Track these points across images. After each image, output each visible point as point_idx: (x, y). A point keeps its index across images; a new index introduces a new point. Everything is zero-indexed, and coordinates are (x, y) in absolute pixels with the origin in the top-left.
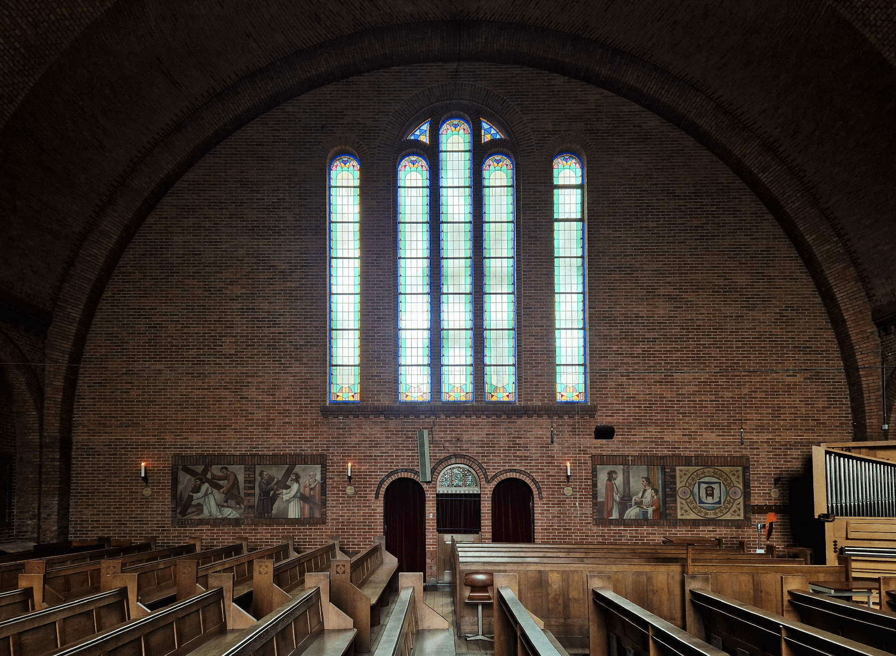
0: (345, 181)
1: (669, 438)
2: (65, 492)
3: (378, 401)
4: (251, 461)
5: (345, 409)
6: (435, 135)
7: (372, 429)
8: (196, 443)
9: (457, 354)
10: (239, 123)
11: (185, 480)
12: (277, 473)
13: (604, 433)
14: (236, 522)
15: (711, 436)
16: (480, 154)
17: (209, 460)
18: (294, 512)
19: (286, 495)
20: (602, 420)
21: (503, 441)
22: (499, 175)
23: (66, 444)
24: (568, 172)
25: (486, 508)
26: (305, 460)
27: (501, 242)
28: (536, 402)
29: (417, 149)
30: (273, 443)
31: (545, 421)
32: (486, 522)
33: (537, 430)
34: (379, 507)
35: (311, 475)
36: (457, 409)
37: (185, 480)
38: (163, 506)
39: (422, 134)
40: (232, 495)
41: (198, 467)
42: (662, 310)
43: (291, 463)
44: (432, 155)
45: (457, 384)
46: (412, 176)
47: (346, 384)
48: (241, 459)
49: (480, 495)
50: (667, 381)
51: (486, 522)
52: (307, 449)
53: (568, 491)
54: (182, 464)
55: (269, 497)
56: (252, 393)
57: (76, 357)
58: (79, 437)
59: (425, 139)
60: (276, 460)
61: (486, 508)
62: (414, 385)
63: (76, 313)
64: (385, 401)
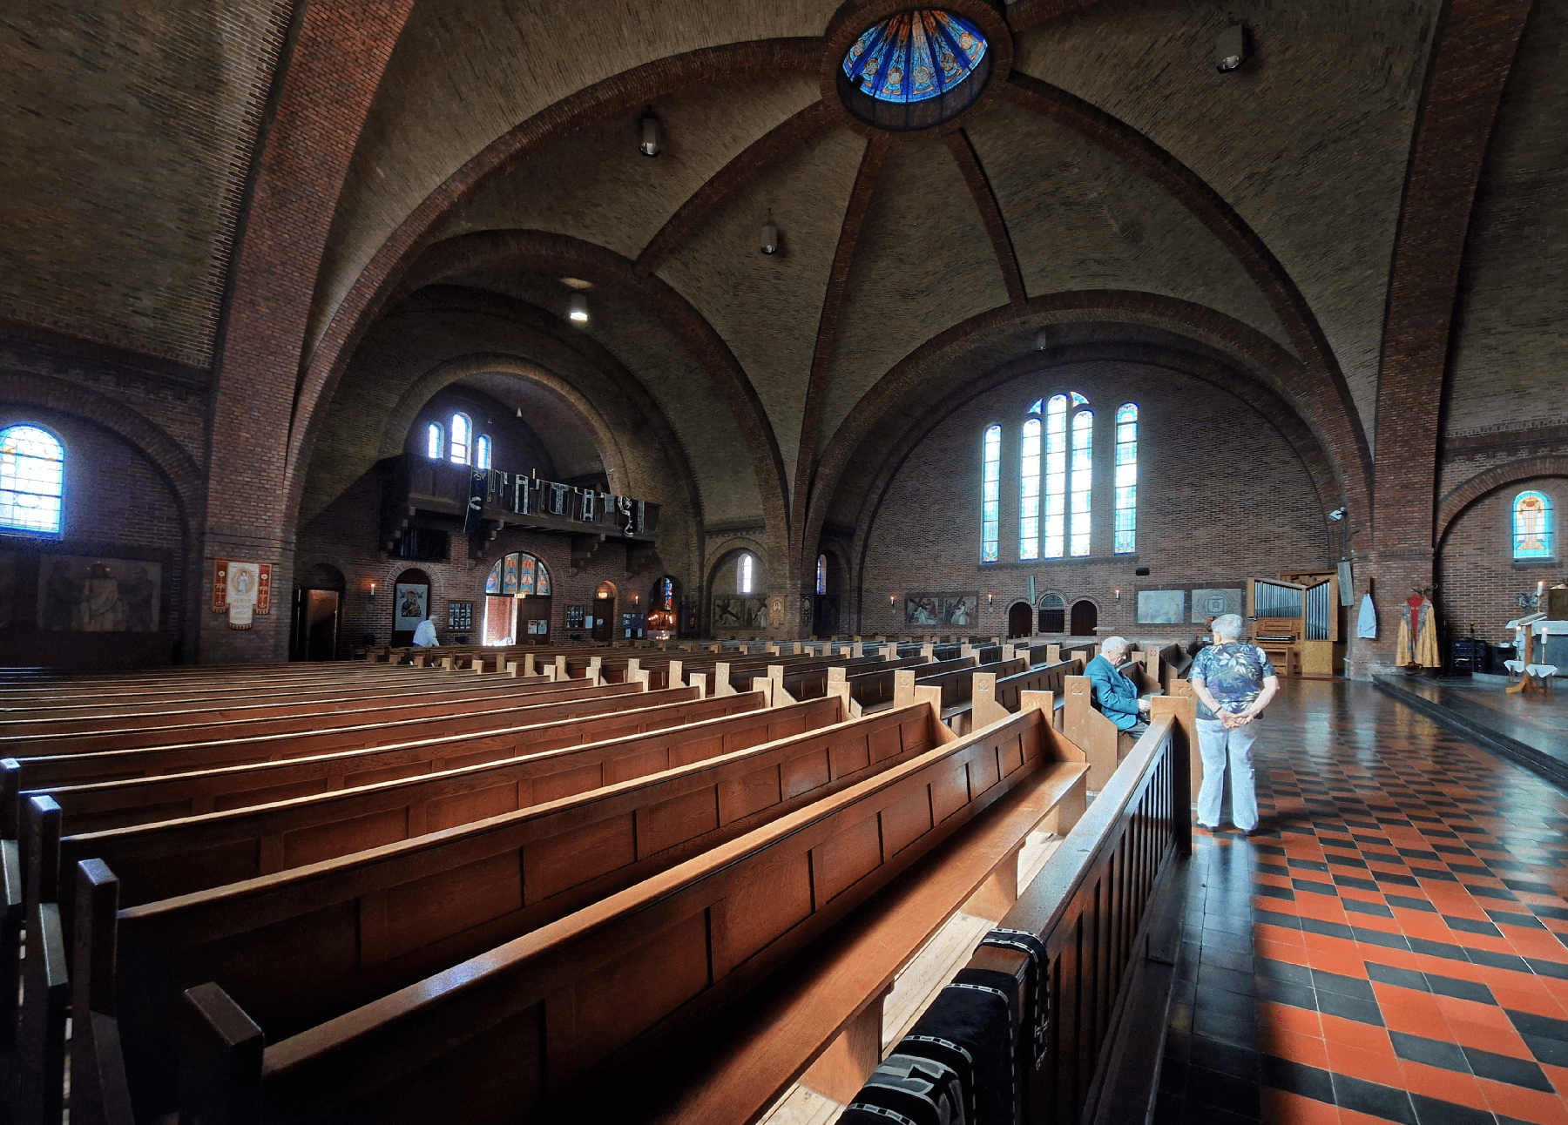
0: (992, 439)
1: (1189, 573)
2: (859, 613)
3: (1009, 563)
4: (939, 595)
5: (990, 566)
6: (1043, 407)
7: (1003, 576)
8: (917, 586)
9: (1054, 526)
10: (939, 422)
11: (911, 605)
12: (954, 601)
13: (1143, 572)
14: (934, 627)
15: (1218, 570)
16: (1071, 412)
17: (923, 595)
18: (962, 621)
19: (958, 612)
20: (1142, 564)
21: (1079, 579)
22: (1084, 421)
23: (860, 589)
24: (1128, 414)
25: (1068, 618)
26: (968, 594)
27: (1029, 506)
28: (1104, 556)
29: (1034, 415)
30: (952, 585)
31: (1105, 566)
32: (1067, 625)
33: (1100, 572)
34: (1006, 618)
35: (971, 602)
36: (1052, 563)
37: (911, 605)
38: (901, 617)
39: (1036, 408)
40: (932, 612)
41: (916, 600)
42: (1187, 492)
43: (961, 597)
44: (1042, 418)
45: (1054, 550)
46: (1031, 429)
47: (990, 550)
48: (937, 595)
49: (917, 683)
50: (1189, 536)
51: (1067, 625)
52: (969, 589)
53: (1119, 607)
54: (910, 598)
55: (950, 614)
56: (942, 560)
57: (865, 547)
58: (865, 586)
59: (1038, 410)
60: (953, 595)
61: (1068, 618)
62: (1029, 550)
63: (865, 527)
64: (1012, 561)
